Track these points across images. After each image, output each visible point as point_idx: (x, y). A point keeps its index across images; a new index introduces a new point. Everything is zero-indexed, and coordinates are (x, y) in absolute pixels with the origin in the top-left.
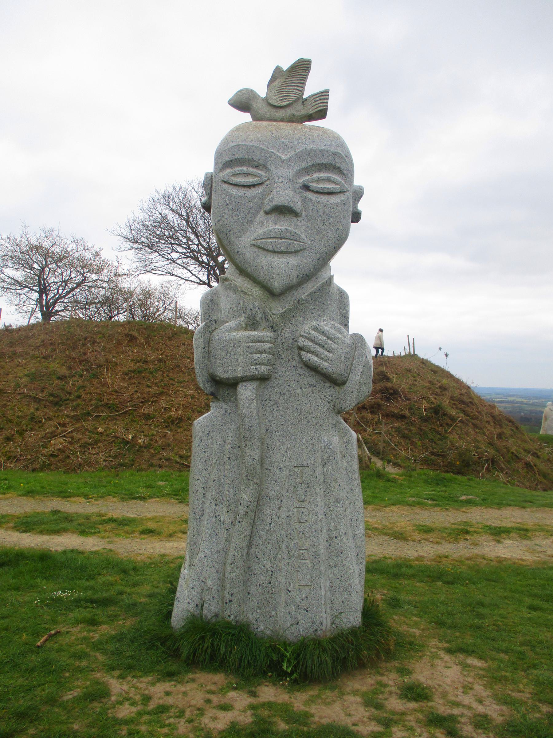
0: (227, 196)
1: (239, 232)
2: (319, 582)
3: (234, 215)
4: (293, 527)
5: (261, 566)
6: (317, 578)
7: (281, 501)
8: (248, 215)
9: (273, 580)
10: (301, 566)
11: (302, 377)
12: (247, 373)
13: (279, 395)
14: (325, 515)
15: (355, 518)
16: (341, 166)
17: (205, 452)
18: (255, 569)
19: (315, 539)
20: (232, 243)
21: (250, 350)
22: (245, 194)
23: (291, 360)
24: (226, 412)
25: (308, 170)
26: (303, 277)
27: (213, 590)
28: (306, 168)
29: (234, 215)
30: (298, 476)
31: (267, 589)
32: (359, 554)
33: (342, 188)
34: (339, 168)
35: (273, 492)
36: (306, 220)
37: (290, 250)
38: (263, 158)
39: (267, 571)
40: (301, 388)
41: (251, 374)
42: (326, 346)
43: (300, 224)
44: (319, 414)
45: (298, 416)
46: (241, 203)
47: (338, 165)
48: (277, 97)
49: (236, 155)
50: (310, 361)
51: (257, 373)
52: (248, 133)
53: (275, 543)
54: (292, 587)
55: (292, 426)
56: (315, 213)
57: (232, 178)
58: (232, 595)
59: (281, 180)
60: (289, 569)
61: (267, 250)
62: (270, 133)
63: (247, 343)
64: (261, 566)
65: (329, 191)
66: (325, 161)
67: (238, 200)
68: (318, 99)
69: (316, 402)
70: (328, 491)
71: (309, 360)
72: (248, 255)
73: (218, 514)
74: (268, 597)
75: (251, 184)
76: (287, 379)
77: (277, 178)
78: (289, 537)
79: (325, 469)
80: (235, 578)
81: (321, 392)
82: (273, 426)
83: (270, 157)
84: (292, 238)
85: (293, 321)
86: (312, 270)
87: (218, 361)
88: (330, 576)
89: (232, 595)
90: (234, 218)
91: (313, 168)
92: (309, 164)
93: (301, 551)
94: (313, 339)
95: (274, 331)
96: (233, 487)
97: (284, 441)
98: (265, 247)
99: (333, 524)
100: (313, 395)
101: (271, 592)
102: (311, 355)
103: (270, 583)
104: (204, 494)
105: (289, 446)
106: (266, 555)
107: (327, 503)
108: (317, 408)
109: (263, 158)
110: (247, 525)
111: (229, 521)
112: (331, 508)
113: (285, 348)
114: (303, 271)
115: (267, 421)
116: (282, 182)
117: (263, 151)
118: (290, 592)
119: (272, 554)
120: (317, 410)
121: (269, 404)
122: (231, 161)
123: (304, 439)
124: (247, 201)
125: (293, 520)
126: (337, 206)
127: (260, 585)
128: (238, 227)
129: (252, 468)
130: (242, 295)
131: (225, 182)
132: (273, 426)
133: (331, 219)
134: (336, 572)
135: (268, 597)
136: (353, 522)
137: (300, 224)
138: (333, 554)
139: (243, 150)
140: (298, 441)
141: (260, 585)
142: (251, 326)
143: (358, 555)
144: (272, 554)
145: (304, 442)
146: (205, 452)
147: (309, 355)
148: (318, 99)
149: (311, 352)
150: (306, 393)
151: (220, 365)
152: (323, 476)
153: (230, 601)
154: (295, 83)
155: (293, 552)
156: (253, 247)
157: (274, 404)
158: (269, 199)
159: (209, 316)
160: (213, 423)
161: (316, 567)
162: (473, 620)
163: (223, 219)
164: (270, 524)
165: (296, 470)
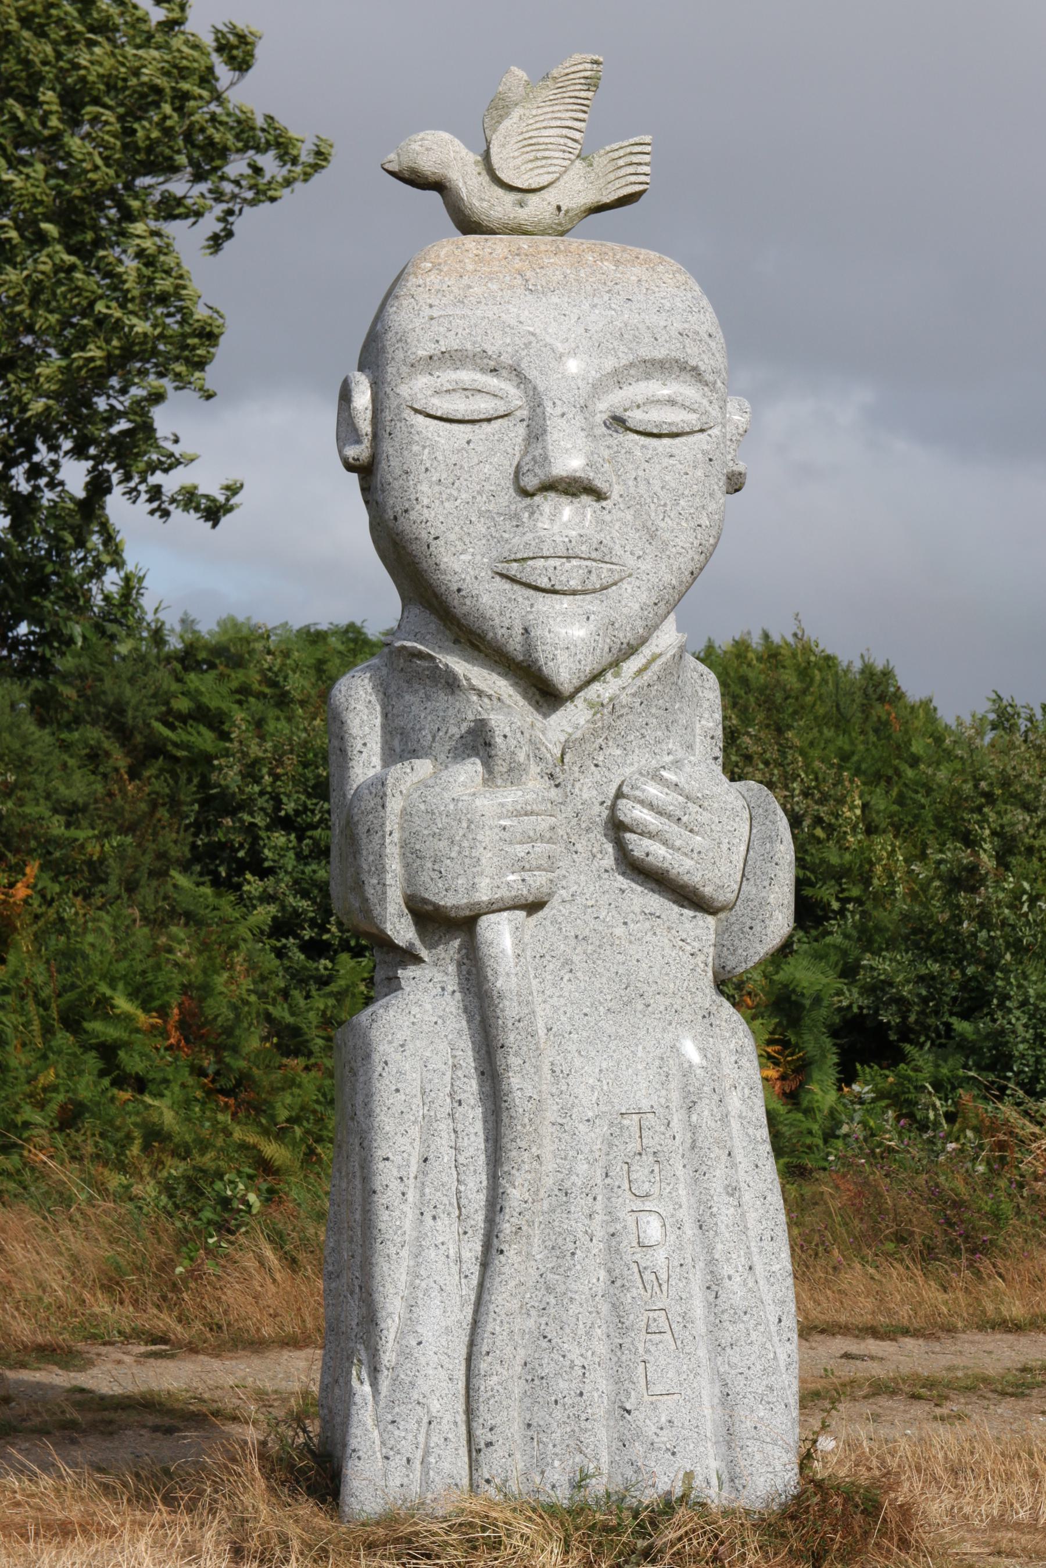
0: (424, 447)
1: (461, 539)
2: (695, 1385)
3: (444, 496)
4: (627, 1258)
5: (556, 1356)
6: (692, 1376)
7: (595, 1199)
8: (479, 498)
9: (587, 1388)
10: (653, 1349)
11: (628, 894)
12: (503, 893)
13: (573, 942)
14: (701, 1227)
15: (767, 1236)
16: (700, 364)
17: (397, 1090)
18: (541, 1365)
19: (681, 1285)
20: (442, 566)
21: (506, 835)
22: (468, 442)
23: (599, 856)
24: (443, 989)
25: (618, 378)
26: (620, 650)
27: (444, 1421)
28: (616, 371)
29: (444, 496)
30: (630, 1137)
31: (574, 1411)
32: (784, 1318)
33: (704, 418)
34: (695, 369)
35: (574, 1178)
36: (622, 506)
37: (590, 587)
38: (509, 349)
39: (572, 1368)
40: (625, 923)
41: (514, 893)
42: (685, 819)
43: (608, 518)
44: (672, 985)
45: (623, 993)
46: (461, 467)
47: (693, 363)
48: (518, 162)
49: (442, 343)
50: (650, 858)
51: (525, 892)
52: (465, 280)
53: (587, 1301)
54: (633, 1400)
55: (610, 1016)
56: (642, 488)
57: (435, 401)
58: (491, 1429)
59: (559, 411)
60: (624, 1358)
61: (537, 588)
62: (519, 281)
63: (500, 818)
64: (556, 1356)
65: (675, 430)
66: (660, 353)
67: (454, 458)
68: (621, 162)
69: (663, 957)
70: (704, 1168)
71: (647, 855)
72: (485, 599)
73: (441, 1239)
74: (577, 1429)
75: (482, 416)
76: (590, 903)
77: (550, 404)
78: (618, 1283)
79: (694, 1118)
80: (498, 1387)
81: (674, 932)
82: (564, 1018)
83: (528, 345)
84: (594, 555)
85: (601, 758)
86: (641, 631)
87: (429, 865)
88: (722, 1370)
89: (491, 1429)
90: (446, 504)
91: (632, 372)
92: (624, 362)
93: (651, 1314)
94: (655, 802)
95: (557, 786)
96: (475, 1171)
97: (593, 1054)
98: (531, 580)
99: (720, 1246)
100: (655, 939)
101: (583, 1417)
102: (651, 842)
103: (581, 1394)
104: (403, 1194)
105: (604, 1065)
106: (567, 1330)
107: (704, 1198)
108: (667, 968)
109: (509, 349)
110: (520, 1259)
111: (469, 1255)
112: (714, 1210)
113: (583, 826)
114: (621, 635)
115: (548, 1006)
116: (563, 415)
117: (507, 330)
118: (629, 1412)
119: (581, 1326)
120: (667, 974)
121: (551, 966)
122: (431, 358)
123: (640, 1047)
124: (476, 461)
125: (625, 1243)
126: (695, 467)
127: (556, 1402)
128: (457, 528)
129: (526, 1120)
130: (475, 698)
131: (417, 411)
132: (564, 1018)
133: (682, 502)
134: (734, 1360)
135: (577, 1429)
136: (764, 1244)
137: (608, 518)
138: (725, 1317)
139: (460, 331)
140: (627, 1052)
141: (556, 1402)
142: (506, 776)
143: (780, 1321)
144: (581, 1326)
145: (639, 1054)
146: (397, 1090)
147: (646, 842)
148: (621, 162)
149: (651, 836)
150: (639, 935)
151: (435, 875)
152: (689, 1134)
153: (489, 1444)
154: (560, 119)
155: (632, 1317)
156: (498, 578)
157: (563, 965)
158: (534, 459)
159: (365, 744)
160: (412, 1019)
161: (687, 1349)
162: (974, 935)
163: (418, 507)
164: (573, 1254)
165: (626, 1122)
